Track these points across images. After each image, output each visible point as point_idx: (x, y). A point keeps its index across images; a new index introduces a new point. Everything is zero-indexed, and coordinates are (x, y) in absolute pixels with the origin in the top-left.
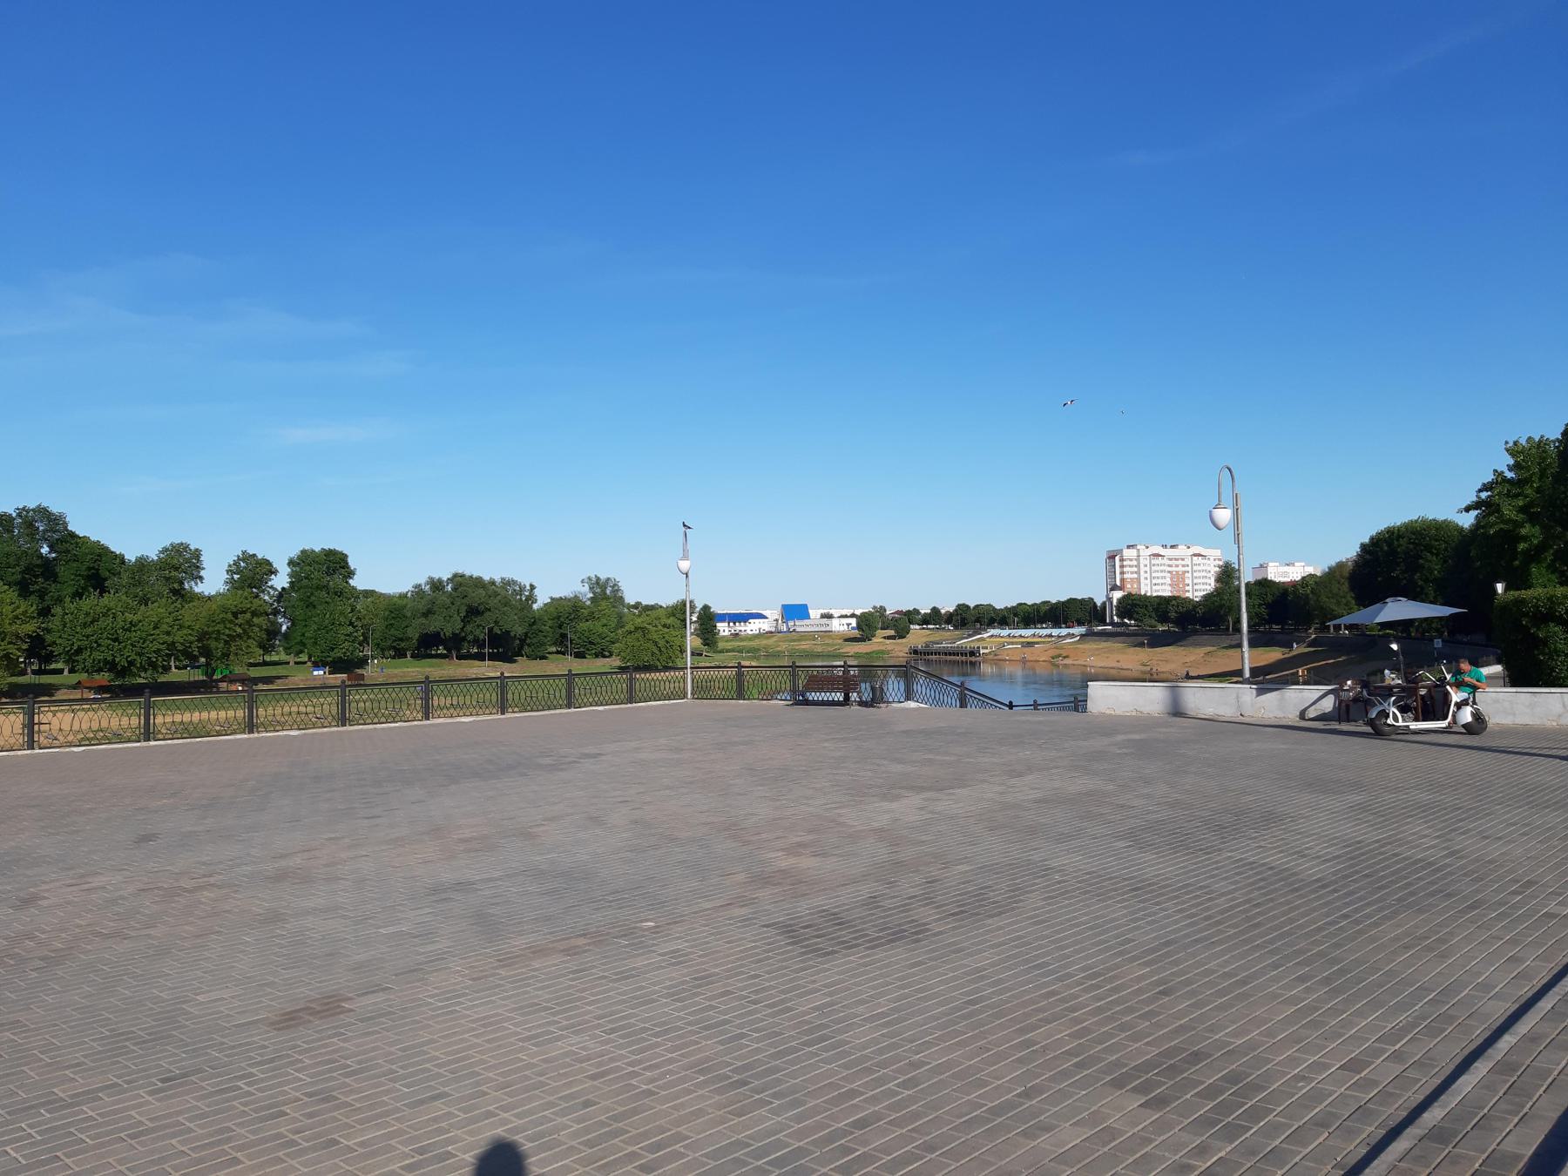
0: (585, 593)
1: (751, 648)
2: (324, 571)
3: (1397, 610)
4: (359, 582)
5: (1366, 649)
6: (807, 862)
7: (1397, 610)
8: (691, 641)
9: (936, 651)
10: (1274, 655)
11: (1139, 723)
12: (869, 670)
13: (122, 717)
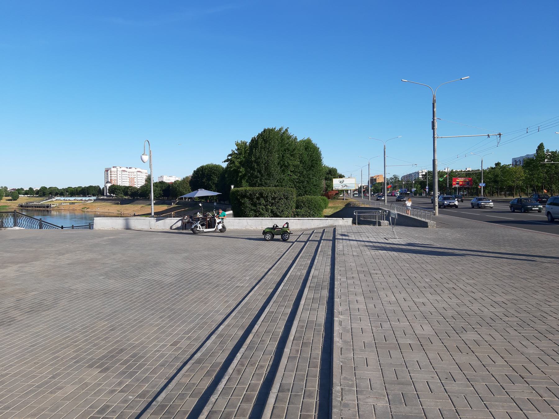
3: (202, 193)
5: (193, 204)
10: (164, 207)
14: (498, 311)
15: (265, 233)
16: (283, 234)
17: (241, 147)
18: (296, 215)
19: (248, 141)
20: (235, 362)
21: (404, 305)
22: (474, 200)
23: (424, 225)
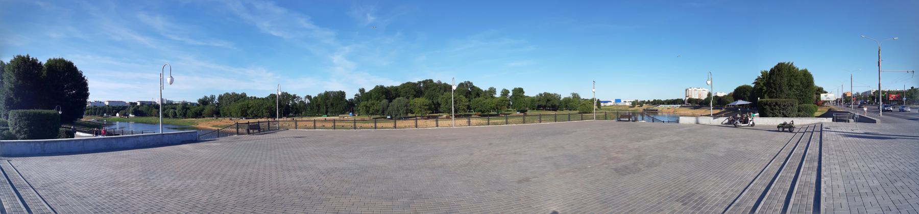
0: (571, 96)
1: (609, 108)
2: (519, 92)
3: (740, 102)
4: (525, 94)
5: (735, 109)
6: (620, 155)
7: (740, 102)
8: (595, 107)
9: (649, 110)
10: (718, 111)
11: (690, 125)
12: (634, 114)
13: (483, 121)
14: (913, 168)
15: (778, 127)
16: (790, 128)
17: (764, 74)
18: (798, 116)
19: (769, 70)
20: (760, 206)
21: (863, 169)
22: (900, 107)
23: (874, 122)
